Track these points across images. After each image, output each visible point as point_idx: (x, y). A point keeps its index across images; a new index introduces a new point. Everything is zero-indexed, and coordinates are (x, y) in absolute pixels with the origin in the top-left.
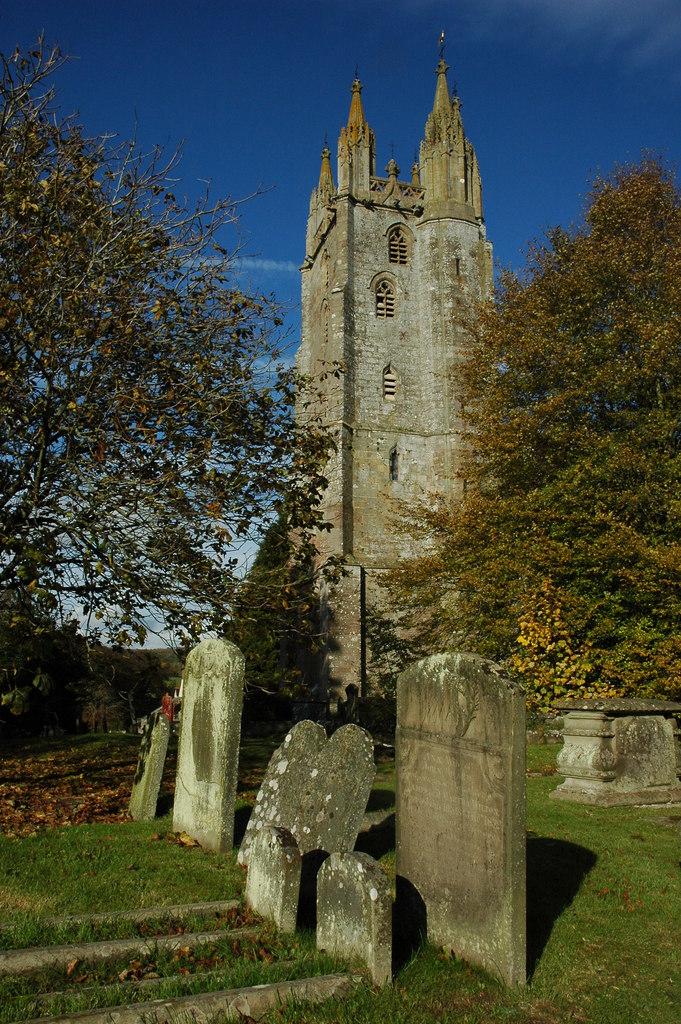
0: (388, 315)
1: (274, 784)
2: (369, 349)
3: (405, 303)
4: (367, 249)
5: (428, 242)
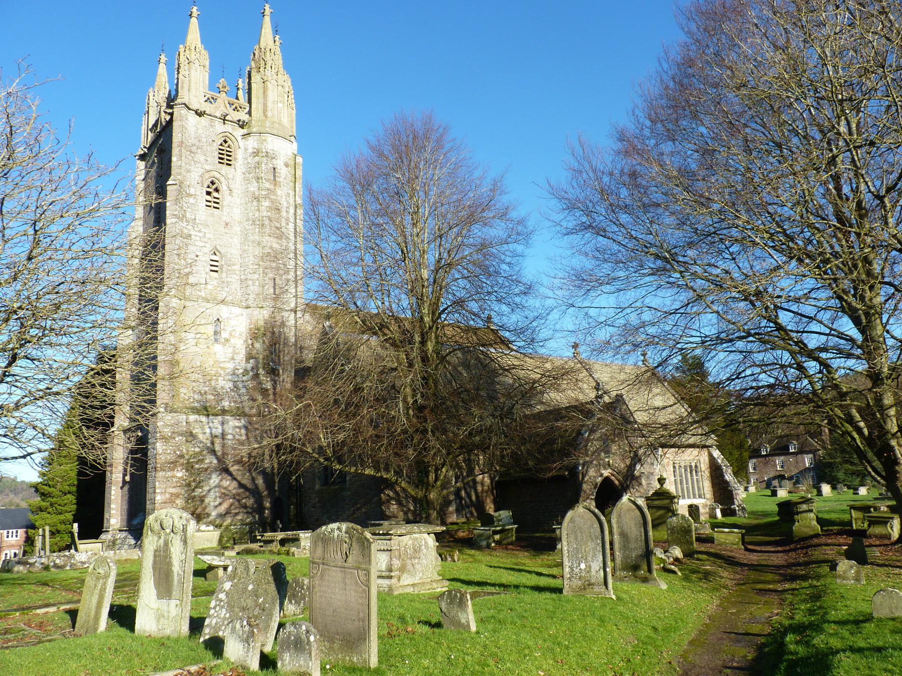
0: (214, 207)
1: (222, 596)
2: (198, 234)
3: (229, 198)
4: (199, 150)
5: (250, 151)
